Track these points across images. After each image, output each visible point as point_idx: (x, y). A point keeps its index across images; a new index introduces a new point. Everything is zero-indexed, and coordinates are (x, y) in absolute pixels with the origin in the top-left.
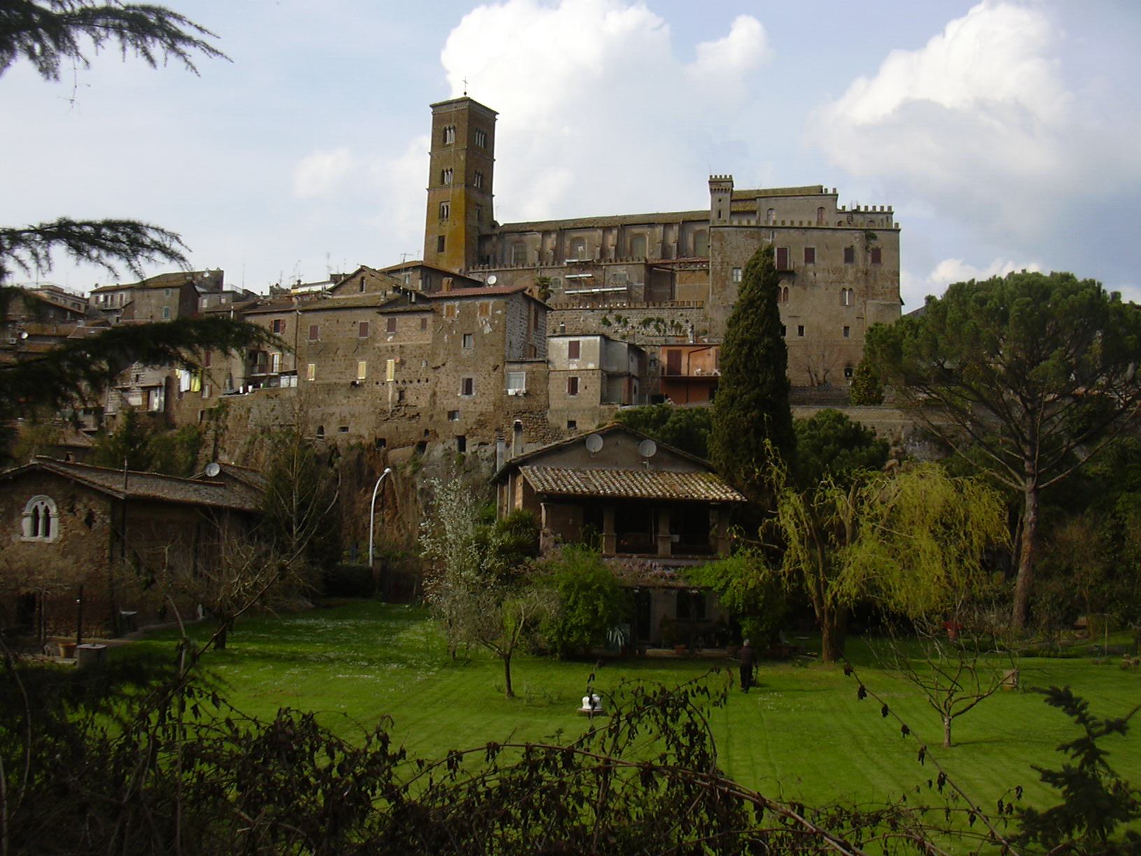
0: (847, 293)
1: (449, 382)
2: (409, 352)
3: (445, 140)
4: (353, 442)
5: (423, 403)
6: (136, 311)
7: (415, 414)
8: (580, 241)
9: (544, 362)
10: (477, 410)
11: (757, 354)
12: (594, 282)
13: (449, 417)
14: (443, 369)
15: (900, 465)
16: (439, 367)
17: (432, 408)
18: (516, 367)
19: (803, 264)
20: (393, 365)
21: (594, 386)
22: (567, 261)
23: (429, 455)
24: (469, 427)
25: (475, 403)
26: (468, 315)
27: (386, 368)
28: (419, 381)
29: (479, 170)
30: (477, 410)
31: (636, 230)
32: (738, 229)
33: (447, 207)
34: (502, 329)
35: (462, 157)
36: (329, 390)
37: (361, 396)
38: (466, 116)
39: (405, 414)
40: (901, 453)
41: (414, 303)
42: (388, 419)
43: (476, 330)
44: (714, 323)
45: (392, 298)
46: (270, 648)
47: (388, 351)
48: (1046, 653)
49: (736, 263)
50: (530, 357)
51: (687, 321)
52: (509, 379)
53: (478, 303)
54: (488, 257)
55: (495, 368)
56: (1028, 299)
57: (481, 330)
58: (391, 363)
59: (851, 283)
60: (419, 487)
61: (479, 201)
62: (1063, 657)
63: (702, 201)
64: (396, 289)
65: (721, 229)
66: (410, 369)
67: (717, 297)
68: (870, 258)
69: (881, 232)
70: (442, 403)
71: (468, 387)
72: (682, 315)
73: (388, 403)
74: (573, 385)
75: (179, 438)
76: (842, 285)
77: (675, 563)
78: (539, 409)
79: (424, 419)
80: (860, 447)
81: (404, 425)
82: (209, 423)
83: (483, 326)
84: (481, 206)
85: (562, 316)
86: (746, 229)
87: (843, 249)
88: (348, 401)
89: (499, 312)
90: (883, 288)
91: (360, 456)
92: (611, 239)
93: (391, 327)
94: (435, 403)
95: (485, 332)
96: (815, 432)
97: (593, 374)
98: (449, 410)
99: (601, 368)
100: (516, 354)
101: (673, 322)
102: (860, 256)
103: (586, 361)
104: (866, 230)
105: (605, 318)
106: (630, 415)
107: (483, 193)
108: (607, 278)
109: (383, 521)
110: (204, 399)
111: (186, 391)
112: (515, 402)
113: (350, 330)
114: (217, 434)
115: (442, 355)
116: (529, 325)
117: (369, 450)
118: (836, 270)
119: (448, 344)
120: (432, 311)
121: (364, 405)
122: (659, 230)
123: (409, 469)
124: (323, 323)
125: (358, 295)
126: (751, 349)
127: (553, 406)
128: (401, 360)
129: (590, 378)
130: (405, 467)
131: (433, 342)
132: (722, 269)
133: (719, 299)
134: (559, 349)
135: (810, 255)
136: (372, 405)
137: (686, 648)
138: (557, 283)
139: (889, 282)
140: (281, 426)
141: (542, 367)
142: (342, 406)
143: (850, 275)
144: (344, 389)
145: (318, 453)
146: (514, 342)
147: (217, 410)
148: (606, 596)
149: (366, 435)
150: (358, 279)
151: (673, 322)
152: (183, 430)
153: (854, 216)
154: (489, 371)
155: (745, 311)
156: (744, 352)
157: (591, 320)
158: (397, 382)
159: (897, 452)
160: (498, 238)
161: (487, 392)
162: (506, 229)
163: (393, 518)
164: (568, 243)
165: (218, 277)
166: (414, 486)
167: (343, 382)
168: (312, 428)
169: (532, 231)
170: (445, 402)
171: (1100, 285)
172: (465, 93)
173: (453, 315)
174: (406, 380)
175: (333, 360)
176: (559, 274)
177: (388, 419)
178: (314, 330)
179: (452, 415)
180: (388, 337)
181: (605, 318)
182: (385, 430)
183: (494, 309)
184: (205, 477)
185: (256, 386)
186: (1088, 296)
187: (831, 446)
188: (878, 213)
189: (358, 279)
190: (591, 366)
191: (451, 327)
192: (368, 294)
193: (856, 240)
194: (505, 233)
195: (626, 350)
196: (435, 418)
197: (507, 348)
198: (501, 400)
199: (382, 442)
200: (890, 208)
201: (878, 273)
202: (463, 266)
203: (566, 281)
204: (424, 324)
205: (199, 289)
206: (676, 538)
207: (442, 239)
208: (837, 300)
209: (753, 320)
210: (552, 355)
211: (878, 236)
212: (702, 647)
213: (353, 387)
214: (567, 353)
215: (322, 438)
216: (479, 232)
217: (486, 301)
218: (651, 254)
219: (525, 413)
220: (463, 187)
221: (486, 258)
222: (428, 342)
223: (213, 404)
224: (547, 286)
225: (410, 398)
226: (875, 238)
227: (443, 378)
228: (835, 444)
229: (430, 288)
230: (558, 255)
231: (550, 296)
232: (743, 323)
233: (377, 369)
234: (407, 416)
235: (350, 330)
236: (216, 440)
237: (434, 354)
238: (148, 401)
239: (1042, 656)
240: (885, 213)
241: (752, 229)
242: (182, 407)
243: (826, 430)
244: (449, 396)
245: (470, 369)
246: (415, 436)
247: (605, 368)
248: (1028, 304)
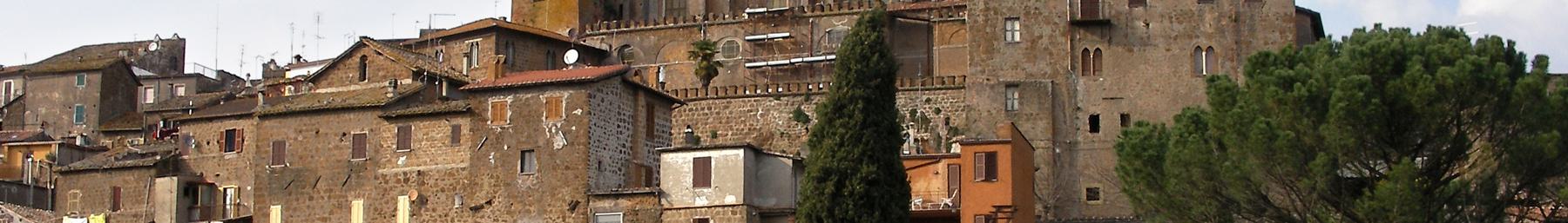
0: (1204, 54)
2: (432, 182)
6: (27, 113)
9: (651, 194)
11: (852, 194)
12: (797, 46)
14: (488, 210)
18: (607, 204)
19: (1127, 7)
20: (408, 204)
22: (748, 10)
26: (528, 118)
27: (396, 209)
34: (583, 140)
41: (447, 99)
45: (409, 91)
47: (398, 181)
49: (1010, 9)
50: (640, 186)
51: (938, 111)
53: (543, 97)
54: (621, 6)
55: (574, 206)
56: (1366, 77)
57: (549, 143)
59: (1209, 36)
64: (417, 75)
66: (434, 210)
67: (979, 68)
72: (928, 101)
76: (1195, 41)
83: (552, 136)
85: (727, 107)
89: (579, 112)
90: (1266, 43)
93: (404, 141)
95: (556, 147)
97: (734, 213)
99: (748, 203)
100: (612, 180)
101: (913, 112)
103: (722, 191)
105: (799, 108)
108: (816, 38)
113: (337, 147)
115: (486, 187)
116: (635, 131)
119: (496, 167)
120: (469, 112)
124: (293, 136)
125: (358, 87)
126: (840, 185)
128: (420, 196)
131: (472, 165)
132: (986, 21)
133: (983, 72)
134: (678, 171)
138: (731, 49)
139: (1277, 34)
141: (649, 204)
143: (1208, 25)
146: (606, 161)
150: (356, 59)
151: (913, 112)
155: (830, 122)
156: (827, 191)
157: (776, 114)
165: (174, 51)
168: (1329, 177)
171: (1511, 43)
173: (503, 118)
175: (311, 198)
176: (736, 34)
178: (279, 146)
180: (398, 157)
181: (799, 108)
183: (570, 108)
186: (1469, 67)
189: (356, 59)
191: (499, 138)
192: (372, 86)
195: (789, 171)
197: (593, 173)
202: (576, 24)
203: (747, 45)
204: (455, 137)
205: (137, 72)
208: (1187, 67)
209: (842, 137)
210: (666, 184)
214: (689, 179)
217: (557, 94)
221: (617, 8)
222: (463, 165)
224: (712, 55)
229: (513, 65)
232: (828, 142)
235: (337, 147)
237: (473, 185)
245: (532, 209)
247: (757, 202)
248: (1361, 86)
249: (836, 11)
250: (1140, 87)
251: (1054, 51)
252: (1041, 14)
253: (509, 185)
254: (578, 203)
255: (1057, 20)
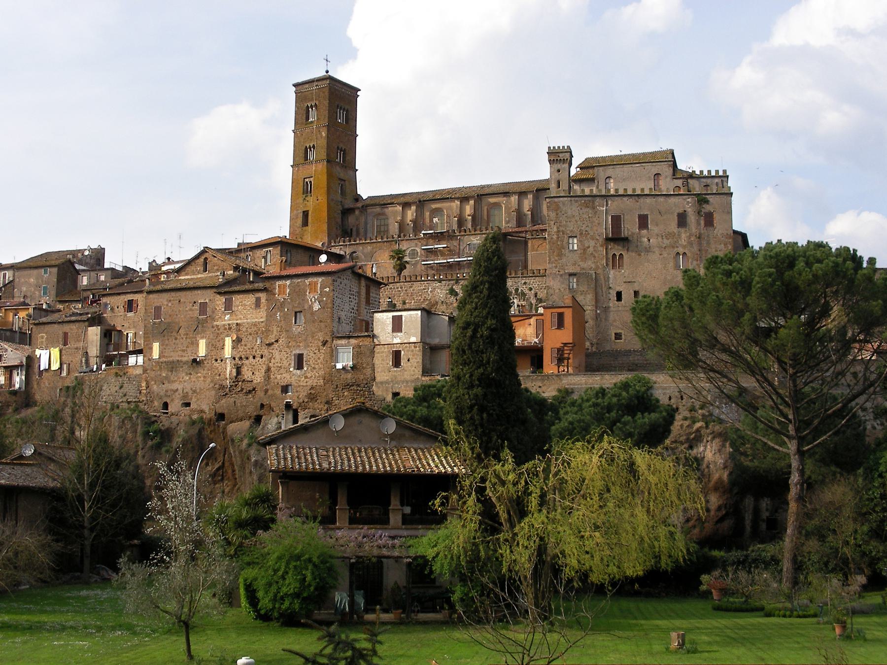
1: (282, 357)
2: (244, 329)
3: (307, 118)
4: (195, 417)
5: (258, 378)
7: (251, 388)
8: (436, 212)
9: (369, 336)
10: (308, 384)
12: (451, 252)
13: (282, 392)
14: (276, 345)
15: (707, 427)
16: (273, 344)
17: (266, 383)
18: (343, 342)
20: (231, 342)
21: (416, 359)
22: (423, 232)
23: (264, 427)
24: (301, 401)
25: (306, 377)
26: (299, 293)
27: (224, 345)
28: (254, 357)
29: (341, 145)
30: (308, 384)
31: (492, 200)
32: (573, 199)
33: (311, 182)
34: (330, 305)
35: (324, 134)
36: (173, 368)
37: (202, 372)
38: (327, 94)
39: (242, 390)
40: (708, 415)
41: (253, 282)
42: (227, 394)
43: (306, 307)
44: (551, 291)
45: (231, 278)
46: (35, 618)
47: (225, 329)
48: (782, 613)
49: (571, 231)
50: (362, 332)
51: (531, 289)
52: (337, 353)
54: (351, 230)
55: (325, 343)
57: (311, 307)
58: (228, 342)
59: (684, 247)
60: (253, 459)
61: (342, 176)
62: (799, 616)
63: (542, 171)
64: (236, 268)
65: (556, 200)
66: (245, 345)
68: (702, 222)
69: (713, 196)
70: (276, 378)
71: (300, 362)
72: (525, 283)
73: (226, 379)
74: (397, 358)
75: (39, 415)
76: (676, 249)
77: (405, 533)
78: (365, 382)
79: (260, 393)
80: (642, 414)
81: (241, 399)
82: (66, 401)
83: (312, 303)
84: (345, 181)
85: (411, 287)
86: (580, 199)
87: (676, 214)
88: (190, 378)
89: (327, 290)
90: (716, 251)
91: (200, 431)
92: (469, 209)
93: (228, 306)
94: (269, 378)
95: (314, 309)
96: (600, 400)
97: (415, 347)
98: (282, 384)
100: (346, 329)
102: (693, 221)
103: (408, 334)
104: (699, 194)
106: (425, 388)
107: (346, 167)
108: (462, 248)
109: (223, 492)
110: (62, 378)
111: (46, 370)
112: (344, 376)
113: (191, 310)
114: (73, 411)
115: (275, 332)
116: (360, 300)
117: (209, 424)
118: (669, 235)
119: (281, 321)
120: (265, 290)
121: (204, 381)
122: (514, 199)
123: (246, 442)
125: (202, 276)
126: (475, 331)
127: (378, 379)
128: (237, 337)
129: (412, 351)
130: (241, 440)
131: (267, 320)
132: (558, 238)
133: (556, 267)
134: (383, 323)
135: (643, 222)
136: (212, 381)
137: (403, 613)
138: (414, 254)
140: (129, 403)
141: (367, 342)
142: (183, 382)
144: (185, 367)
145: (162, 428)
146: (343, 317)
147: (74, 388)
148: (315, 565)
149: (207, 410)
150: (202, 259)
151: (517, 290)
152: (43, 408)
153: (689, 181)
154: (318, 346)
155: (470, 295)
157: (439, 291)
158: (234, 359)
159: (703, 415)
160: (361, 212)
161: (317, 366)
162: (368, 202)
163: (232, 489)
164: (427, 214)
165: (99, 255)
166: (249, 459)
167: (185, 359)
168: (157, 404)
169: (392, 203)
170: (279, 377)
172: (327, 72)
173: (284, 293)
174: (243, 357)
175: (176, 339)
177: (227, 394)
178: (158, 309)
179: (285, 389)
180: (225, 315)
182: (224, 405)
183: (322, 288)
184: (21, 457)
185: (109, 364)
187: (613, 414)
188: (713, 177)
189: (202, 259)
190: (413, 339)
191: (282, 305)
192: (210, 275)
193: (688, 205)
194: (367, 206)
195: (447, 323)
196: (270, 392)
197: (335, 324)
198: (331, 375)
199: (221, 416)
200: (725, 171)
201: (711, 237)
202: (326, 240)
203: (423, 251)
205: (78, 267)
206: (408, 510)
207: (306, 214)
209: (476, 304)
210: (377, 330)
211: (711, 200)
212: (418, 612)
213: (194, 364)
214: (390, 328)
215: (167, 413)
216: (343, 206)
217: (315, 279)
218: (507, 222)
219: (353, 385)
220: (325, 163)
221: (349, 231)
222: (262, 320)
223: (68, 383)
224: (403, 257)
225: (247, 374)
226: (707, 202)
227: (277, 354)
228: (618, 412)
230: (417, 226)
231: (405, 268)
232: (468, 307)
233: (216, 346)
234: (244, 391)
235: (191, 310)
236: (73, 416)
237: (268, 331)
238: (10, 379)
239: (779, 616)
240: (720, 177)
241: (587, 199)
242: (42, 385)
243: (609, 398)
244: (282, 371)
246: (252, 410)
247: (428, 341)
248: (770, 275)
249: (473, 233)
250: (645, 276)
251: (596, 255)
252: (589, 234)
253: (288, 331)
254: (327, 341)
255: (598, 237)
